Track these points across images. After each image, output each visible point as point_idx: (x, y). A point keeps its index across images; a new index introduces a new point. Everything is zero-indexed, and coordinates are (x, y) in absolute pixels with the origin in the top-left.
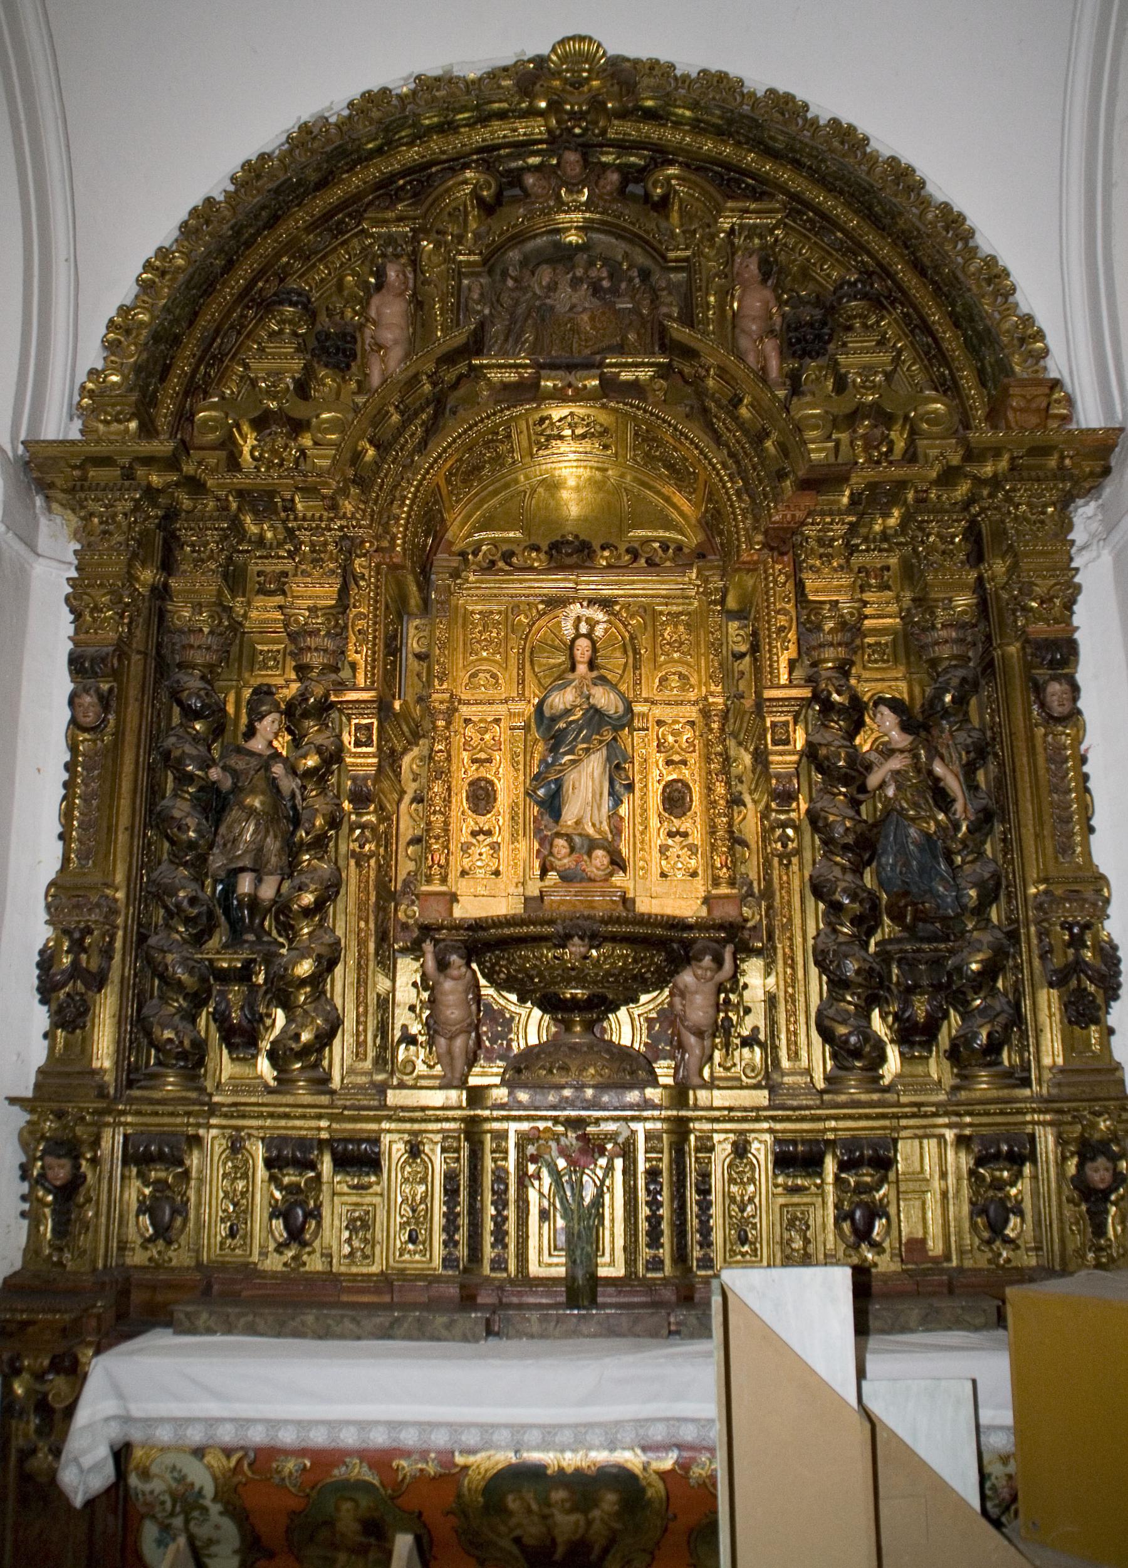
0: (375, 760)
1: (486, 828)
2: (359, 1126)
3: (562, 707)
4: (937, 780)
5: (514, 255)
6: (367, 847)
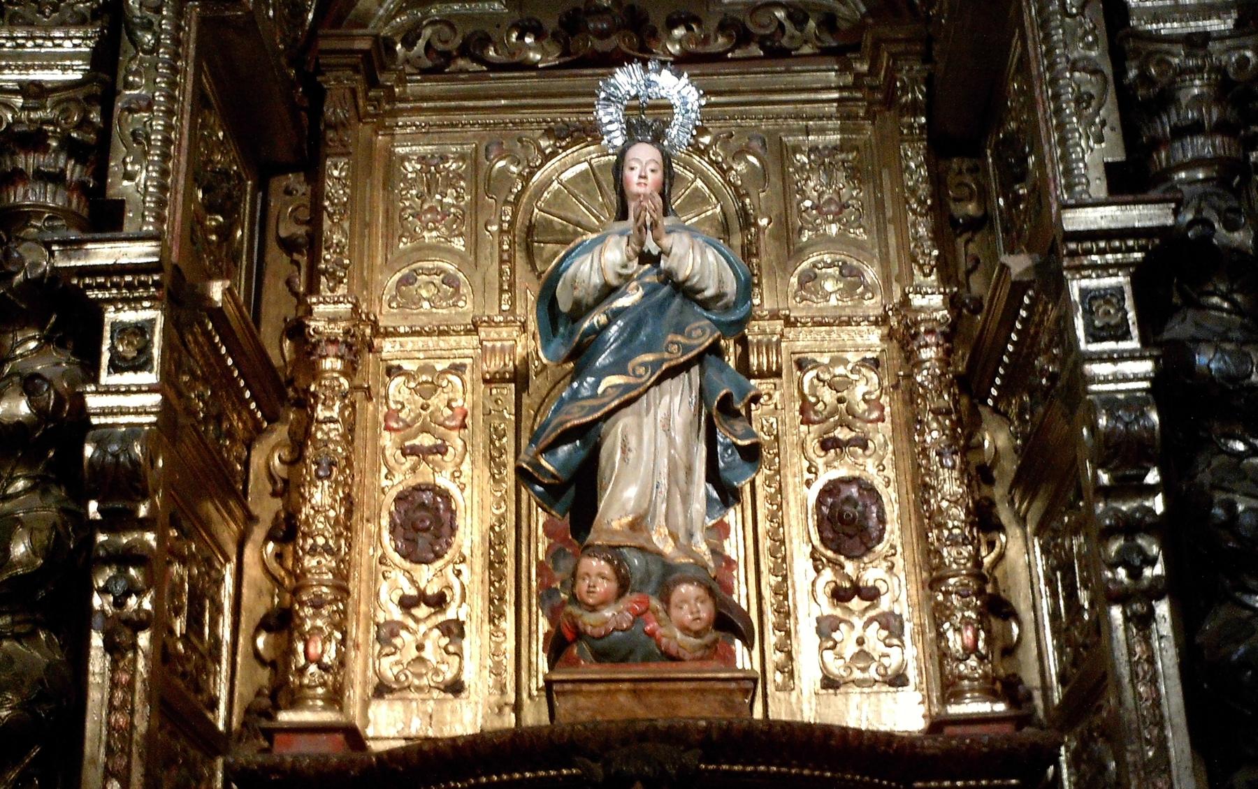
0: (156, 398)
1: (432, 590)
2: (354, 623)
3: (596, 280)
4: (1166, 738)
5: (497, 476)
6: (132, 602)
